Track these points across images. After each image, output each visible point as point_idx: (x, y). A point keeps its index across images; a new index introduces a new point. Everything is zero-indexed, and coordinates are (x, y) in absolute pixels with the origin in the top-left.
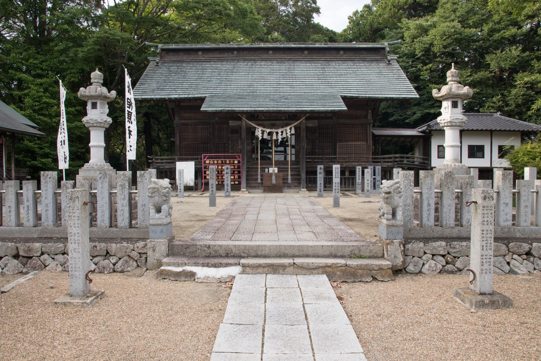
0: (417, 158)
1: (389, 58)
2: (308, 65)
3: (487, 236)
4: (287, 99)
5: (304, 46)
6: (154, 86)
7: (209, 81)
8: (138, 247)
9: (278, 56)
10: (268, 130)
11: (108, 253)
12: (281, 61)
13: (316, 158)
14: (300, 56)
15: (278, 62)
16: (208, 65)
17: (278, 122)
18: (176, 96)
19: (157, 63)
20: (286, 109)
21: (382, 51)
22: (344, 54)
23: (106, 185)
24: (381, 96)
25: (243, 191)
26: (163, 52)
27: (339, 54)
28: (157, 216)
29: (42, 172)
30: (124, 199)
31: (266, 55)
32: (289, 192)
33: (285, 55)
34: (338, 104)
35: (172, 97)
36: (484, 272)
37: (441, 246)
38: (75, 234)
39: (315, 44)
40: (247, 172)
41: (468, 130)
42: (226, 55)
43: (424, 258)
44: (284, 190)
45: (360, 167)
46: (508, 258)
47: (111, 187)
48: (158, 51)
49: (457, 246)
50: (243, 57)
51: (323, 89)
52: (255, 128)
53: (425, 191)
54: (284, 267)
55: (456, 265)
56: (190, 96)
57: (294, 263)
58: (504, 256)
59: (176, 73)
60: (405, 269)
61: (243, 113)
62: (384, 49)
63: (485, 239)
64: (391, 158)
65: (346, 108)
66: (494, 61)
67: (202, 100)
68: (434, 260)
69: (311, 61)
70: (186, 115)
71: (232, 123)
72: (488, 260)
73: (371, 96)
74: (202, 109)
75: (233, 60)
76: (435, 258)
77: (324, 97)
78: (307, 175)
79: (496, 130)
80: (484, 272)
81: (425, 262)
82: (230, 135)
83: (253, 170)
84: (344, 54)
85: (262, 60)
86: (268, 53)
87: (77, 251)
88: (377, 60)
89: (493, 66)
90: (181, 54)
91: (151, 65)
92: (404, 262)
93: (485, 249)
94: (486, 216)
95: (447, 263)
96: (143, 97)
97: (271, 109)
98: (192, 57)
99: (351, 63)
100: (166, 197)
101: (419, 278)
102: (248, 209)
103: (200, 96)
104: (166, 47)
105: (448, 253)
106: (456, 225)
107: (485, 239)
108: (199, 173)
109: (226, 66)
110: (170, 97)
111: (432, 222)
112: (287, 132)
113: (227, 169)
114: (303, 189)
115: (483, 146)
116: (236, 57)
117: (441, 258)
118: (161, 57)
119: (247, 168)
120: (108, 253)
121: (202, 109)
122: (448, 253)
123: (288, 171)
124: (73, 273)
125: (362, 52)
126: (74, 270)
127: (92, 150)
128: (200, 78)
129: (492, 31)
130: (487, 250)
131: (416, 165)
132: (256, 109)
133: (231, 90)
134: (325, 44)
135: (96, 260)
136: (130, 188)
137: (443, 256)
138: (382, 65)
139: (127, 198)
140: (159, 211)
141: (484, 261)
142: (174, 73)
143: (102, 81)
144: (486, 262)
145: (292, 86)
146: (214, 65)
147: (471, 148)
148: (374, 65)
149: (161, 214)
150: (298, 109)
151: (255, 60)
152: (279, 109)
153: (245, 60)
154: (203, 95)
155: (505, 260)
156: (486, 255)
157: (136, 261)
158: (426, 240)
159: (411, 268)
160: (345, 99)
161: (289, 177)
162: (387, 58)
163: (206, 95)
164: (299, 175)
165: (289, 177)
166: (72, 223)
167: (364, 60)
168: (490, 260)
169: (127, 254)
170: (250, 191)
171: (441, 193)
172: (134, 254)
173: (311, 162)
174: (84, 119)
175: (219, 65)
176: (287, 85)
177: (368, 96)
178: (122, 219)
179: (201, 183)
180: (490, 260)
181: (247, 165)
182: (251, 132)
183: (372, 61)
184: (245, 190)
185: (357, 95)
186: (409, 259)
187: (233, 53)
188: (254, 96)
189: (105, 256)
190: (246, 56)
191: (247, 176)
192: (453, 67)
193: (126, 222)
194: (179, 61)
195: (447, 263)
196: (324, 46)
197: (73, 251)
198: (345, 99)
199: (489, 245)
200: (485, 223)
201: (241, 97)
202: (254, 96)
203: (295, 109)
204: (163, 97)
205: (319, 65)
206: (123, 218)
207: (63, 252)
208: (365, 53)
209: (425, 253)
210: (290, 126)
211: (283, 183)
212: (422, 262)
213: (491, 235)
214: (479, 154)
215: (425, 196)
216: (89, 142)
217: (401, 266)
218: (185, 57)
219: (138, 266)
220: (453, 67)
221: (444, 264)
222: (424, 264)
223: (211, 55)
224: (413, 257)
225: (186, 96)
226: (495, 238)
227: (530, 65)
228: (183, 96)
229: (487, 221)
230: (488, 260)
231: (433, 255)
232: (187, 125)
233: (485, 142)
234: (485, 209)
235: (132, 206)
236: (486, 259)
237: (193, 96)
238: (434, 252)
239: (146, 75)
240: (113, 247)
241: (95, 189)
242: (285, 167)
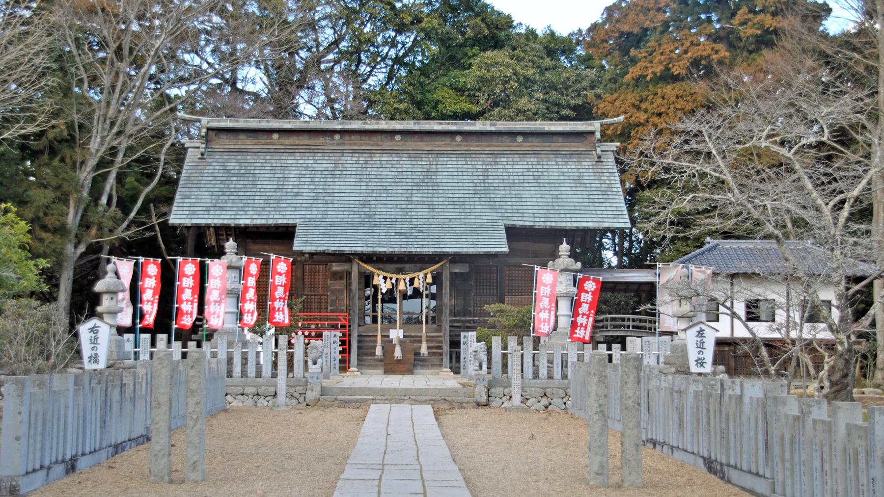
4: (421, 231)
7: (297, 194)
12: (415, 154)
13: (469, 321)
16: (290, 160)
17: (407, 266)
18: (248, 222)
20: (418, 250)
22: (524, 141)
24: (569, 224)
25: (353, 371)
26: (210, 132)
29: (463, 334)
31: (389, 143)
33: (422, 144)
34: (497, 242)
40: (359, 342)
43: (504, 398)
44: (415, 371)
46: (565, 400)
50: (350, 144)
61: (356, 254)
62: (592, 133)
64: (645, 321)
71: (336, 267)
78: (451, 347)
82: (329, 282)
83: (368, 339)
84: (524, 141)
86: (393, 139)
90: (242, 136)
97: (396, 249)
101: (487, 408)
104: (215, 124)
110: (237, 222)
112: (422, 278)
113: (335, 336)
114: (445, 369)
116: (338, 144)
125: (555, 138)
132: (376, 249)
134: (491, 125)
135: (268, 398)
142: (234, 175)
143: (235, 251)
145: (431, 207)
150: (436, 250)
154: (291, 222)
163: (295, 221)
164: (440, 348)
170: (363, 371)
172: (296, 394)
173: (460, 327)
182: (367, 280)
184: (355, 369)
185: (532, 224)
187: (333, 139)
191: (359, 348)
194: (239, 151)
203: (433, 250)
204: (226, 222)
208: (561, 139)
210: (425, 271)
211: (415, 360)
225: (263, 222)
233: (775, 293)
239: (188, 179)
242: (419, 334)
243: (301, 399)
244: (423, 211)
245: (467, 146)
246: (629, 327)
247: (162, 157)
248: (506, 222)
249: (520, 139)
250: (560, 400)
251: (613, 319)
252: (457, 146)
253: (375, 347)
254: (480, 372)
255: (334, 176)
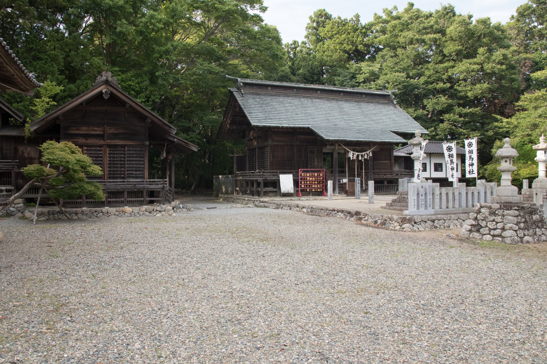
9: (324, 96)
10: (357, 153)
21: (388, 97)
32: (242, 201)
42: (288, 91)
52: (348, 152)
66: (430, 103)
70: (276, 138)
79: (433, 153)
86: (317, 93)
89: (430, 107)
98: (264, 92)
108: (296, 183)
115: (442, 164)
129: (426, 83)
147: (436, 165)
167: (379, 103)
174: (535, 159)
179: (300, 189)
204: (277, 125)
214: (440, 169)
218: (259, 91)
223: (278, 91)
227: (453, 109)
232: (278, 146)
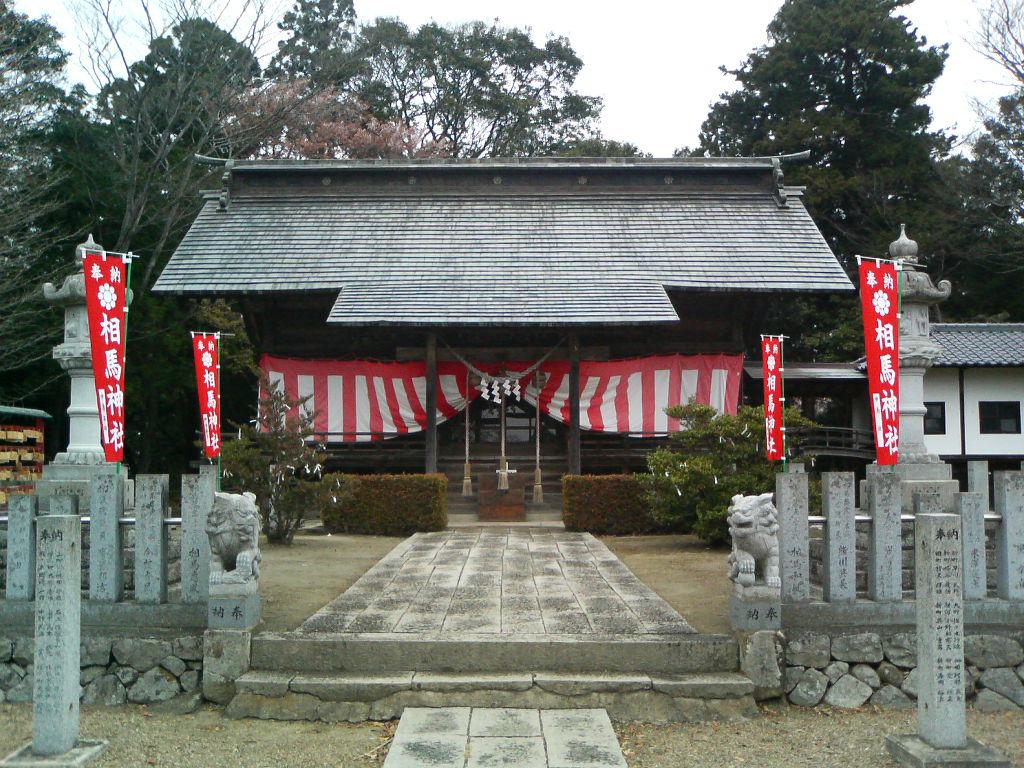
0: (857, 433)
1: (783, 193)
2: (588, 210)
3: (950, 617)
5: (578, 165)
6: (214, 260)
8: (181, 647)
11: (112, 659)
12: (523, 201)
14: (569, 191)
15: (514, 204)
16: (345, 210)
18: (268, 287)
19: (223, 205)
22: (674, 183)
23: (112, 507)
24: (762, 286)
27: (664, 184)
28: (229, 575)
30: (152, 537)
35: (258, 288)
36: (946, 697)
37: (868, 643)
38: (50, 614)
39: (604, 161)
41: (976, 366)
43: (831, 669)
45: (140, 594)
47: (122, 509)
48: (226, 175)
49: (906, 643)
51: (625, 273)
53: (833, 519)
54: (513, 689)
55: (905, 687)
56: (301, 287)
57: (535, 683)
58: (1016, 666)
59: (268, 228)
60: (788, 694)
62: (770, 171)
63: (943, 624)
65: (675, 318)
67: (331, 295)
68: (854, 675)
69: (595, 201)
72: (953, 671)
73: (738, 285)
74: (329, 320)
75: (406, 199)
76: (857, 670)
77: (623, 293)
80: (946, 697)
81: (833, 681)
84: (674, 183)
85: (478, 199)
87: (53, 651)
88: (754, 199)
91: (208, 209)
92: (784, 680)
93: (944, 646)
94: (943, 573)
95: (884, 681)
96: (188, 288)
97: (495, 320)
99: (691, 207)
100: (248, 533)
102: (192, 570)
103: (325, 286)
105: (886, 659)
106: (905, 596)
107: (943, 624)
109: (389, 214)
110: (251, 288)
111: (850, 591)
116: (414, 191)
117: (869, 671)
118: (233, 191)
119: (439, 461)
120: (112, 659)
121: (329, 320)
122: (886, 659)
123: (535, 467)
124: (43, 701)
126: (44, 694)
127: (75, 425)
128: (325, 243)
130: (948, 647)
131: (856, 451)
132: (461, 320)
133: (398, 276)
136: (165, 514)
137: (875, 666)
138: (767, 209)
139: (158, 536)
140: (230, 564)
141: (945, 672)
144: (949, 675)
145: (548, 265)
146: (359, 210)
148: (747, 209)
149: (234, 572)
150: (560, 320)
151: (460, 201)
152: (515, 320)
153: (435, 199)
154: (333, 286)
155: (1019, 677)
156: (948, 660)
157: (178, 679)
158: (834, 629)
159: (802, 690)
160: (676, 295)
161: (538, 486)
162: (777, 194)
163: (339, 285)
165: (538, 486)
166: (46, 588)
167: (723, 199)
168: (957, 671)
169: (158, 661)
171: (871, 522)
172: (174, 663)
175: (372, 211)
176: (535, 260)
177: (730, 285)
178: (144, 582)
180: (957, 671)
181: (438, 456)
183: (743, 200)
185: (705, 285)
186: (794, 673)
188: (455, 289)
189: (107, 666)
190: (436, 190)
192: (903, 232)
193: (154, 592)
195: (884, 681)
196: (624, 165)
197: (44, 653)
198: (676, 295)
199: (953, 636)
200: (944, 589)
201: (425, 290)
202: (455, 285)
203: (555, 320)
205: (614, 213)
206: (148, 586)
207: (7, 659)
209: (833, 659)
212: (825, 680)
213: (956, 616)
214: (1008, 423)
215: (833, 530)
216: (67, 403)
217: (777, 689)
218: (290, 193)
219: (182, 690)
220: (903, 232)
221: (877, 682)
222: (830, 685)
224: (806, 668)
225: (292, 287)
226: (966, 627)
228: (284, 287)
229: (948, 584)
230: (953, 671)
231: (852, 664)
234: (942, 558)
235: (170, 556)
236: (948, 667)
237: (309, 287)
238: (855, 657)
239: (196, 234)
240: (127, 644)
241: (87, 513)
242: (531, 458)
243: (189, 680)
244: (538, 271)
245: (593, 190)
246: (824, 443)
247: (539, 470)
248: (665, 283)
249: (669, 181)
250: (1008, 673)
251: (832, 433)
252: (581, 190)
253: (462, 478)
254: (761, 590)
255: (405, 229)
